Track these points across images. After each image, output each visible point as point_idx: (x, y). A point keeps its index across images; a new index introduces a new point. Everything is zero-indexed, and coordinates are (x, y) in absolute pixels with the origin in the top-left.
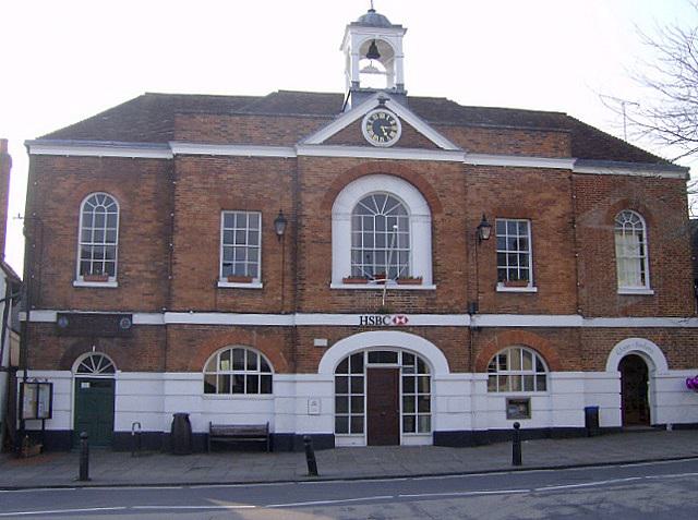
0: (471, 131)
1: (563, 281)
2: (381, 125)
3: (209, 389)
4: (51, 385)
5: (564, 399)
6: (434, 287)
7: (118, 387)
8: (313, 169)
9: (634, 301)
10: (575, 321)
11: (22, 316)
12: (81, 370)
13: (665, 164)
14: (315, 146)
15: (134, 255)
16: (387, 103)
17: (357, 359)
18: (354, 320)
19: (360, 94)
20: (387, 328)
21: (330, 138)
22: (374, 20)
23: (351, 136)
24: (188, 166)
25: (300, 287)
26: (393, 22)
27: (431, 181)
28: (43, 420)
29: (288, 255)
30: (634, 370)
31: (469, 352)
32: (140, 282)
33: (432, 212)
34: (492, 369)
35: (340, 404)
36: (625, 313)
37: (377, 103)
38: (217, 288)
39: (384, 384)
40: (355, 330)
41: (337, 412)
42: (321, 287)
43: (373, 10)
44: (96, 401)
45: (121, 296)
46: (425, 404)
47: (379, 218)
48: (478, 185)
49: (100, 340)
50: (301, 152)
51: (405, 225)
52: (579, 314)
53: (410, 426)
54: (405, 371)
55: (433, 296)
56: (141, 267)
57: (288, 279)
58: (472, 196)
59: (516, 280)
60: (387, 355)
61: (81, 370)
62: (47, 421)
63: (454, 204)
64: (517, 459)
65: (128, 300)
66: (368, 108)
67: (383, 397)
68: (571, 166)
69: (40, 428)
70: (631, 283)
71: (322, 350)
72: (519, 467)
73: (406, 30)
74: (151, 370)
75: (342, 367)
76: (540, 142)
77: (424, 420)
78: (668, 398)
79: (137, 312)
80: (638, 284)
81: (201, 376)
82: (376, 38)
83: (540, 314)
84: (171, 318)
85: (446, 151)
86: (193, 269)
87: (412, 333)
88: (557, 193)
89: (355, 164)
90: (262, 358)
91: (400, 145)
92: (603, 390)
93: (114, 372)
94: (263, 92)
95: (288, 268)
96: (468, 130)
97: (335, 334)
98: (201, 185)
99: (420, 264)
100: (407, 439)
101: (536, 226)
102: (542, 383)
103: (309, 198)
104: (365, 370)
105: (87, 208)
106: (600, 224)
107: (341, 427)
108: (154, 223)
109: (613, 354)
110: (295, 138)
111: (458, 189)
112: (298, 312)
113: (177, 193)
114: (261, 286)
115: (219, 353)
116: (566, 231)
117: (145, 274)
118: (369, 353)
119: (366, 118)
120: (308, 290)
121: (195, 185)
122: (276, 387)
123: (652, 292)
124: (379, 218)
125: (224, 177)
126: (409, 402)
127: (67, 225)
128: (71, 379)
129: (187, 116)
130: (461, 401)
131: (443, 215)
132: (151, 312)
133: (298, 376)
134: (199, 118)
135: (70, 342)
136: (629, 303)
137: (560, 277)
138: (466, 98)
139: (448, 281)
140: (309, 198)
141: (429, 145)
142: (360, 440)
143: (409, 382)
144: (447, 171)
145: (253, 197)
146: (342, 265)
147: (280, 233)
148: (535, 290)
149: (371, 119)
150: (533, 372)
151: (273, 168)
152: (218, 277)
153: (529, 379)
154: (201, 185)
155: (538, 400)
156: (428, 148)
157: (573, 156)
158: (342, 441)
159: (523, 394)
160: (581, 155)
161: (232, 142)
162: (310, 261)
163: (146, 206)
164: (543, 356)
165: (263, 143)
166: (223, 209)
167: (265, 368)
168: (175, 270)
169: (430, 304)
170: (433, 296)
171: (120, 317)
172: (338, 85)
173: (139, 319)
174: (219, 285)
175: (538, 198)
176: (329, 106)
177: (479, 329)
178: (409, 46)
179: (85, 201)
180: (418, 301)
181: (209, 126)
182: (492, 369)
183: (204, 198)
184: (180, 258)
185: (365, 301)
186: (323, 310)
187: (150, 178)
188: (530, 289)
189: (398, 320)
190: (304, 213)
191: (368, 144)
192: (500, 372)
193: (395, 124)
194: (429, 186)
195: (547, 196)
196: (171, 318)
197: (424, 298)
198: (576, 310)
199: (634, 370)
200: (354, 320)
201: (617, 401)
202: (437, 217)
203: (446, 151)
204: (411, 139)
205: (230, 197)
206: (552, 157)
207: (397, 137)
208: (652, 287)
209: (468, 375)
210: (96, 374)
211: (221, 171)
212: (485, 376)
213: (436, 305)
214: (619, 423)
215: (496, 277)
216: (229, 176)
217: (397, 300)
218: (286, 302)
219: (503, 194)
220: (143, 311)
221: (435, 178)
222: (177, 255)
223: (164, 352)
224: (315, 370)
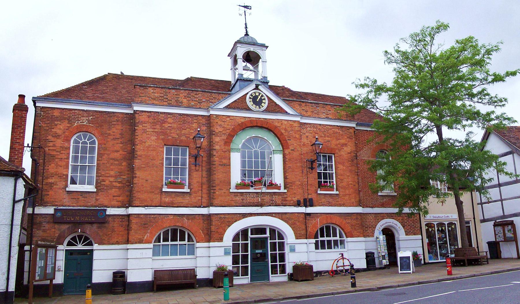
0: (304, 104)
1: (352, 188)
6: (286, 191)
8: (219, 123)
10: (358, 210)
11: (30, 211)
14: (220, 109)
15: (107, 172)
16: (260, 87)
17: (244, 233)
19: (243, 81)
21: (229, 105)
22: (246, 40)
23: (240, 105)
25: (212, 191)
26: (260, 41)
27: (283, 131)
30: (389, 233)
31: (303, 227)
32: (111, 188)
33: (283, 148)
34: (316, 237)
36: (383, 205)
37: (254, 86)
38: (162, 192)
40: (251, 215)
44: (80, 264)
45: (98, 198)
48: (307, 134)
50: (212, 112)
52: (360, 206)
53: (274, 272)
55: (285, 196)
56: (112, 179)
58: (304, 140)
60: (261, 230)
61: (69, 244)
63: (295, 144)
64: (354, 285)
65: (103, 199)
67: (259, 253)
68: (354, 125)
73: (267, 47)
74: (118, 243)
75: (236, 238)
81: (314, 241)
83: (341, 206)
84: (132, 210)
85: (291, 115)
86: (147, 180)
88: (348, 140)
89: (243, 121)
91: (267, 111)
93: (92, 245)
95: (205, 180)
96: (302, 104)
98: (152, 130)
99: (278, 178)
100: (274, 278)
101: (337, 158)
103: (217, 139)
104: (249, 239)
105: (76, 142)
106: (369, 157)
108: (121, 152)
109: (377, 227)
111: (297, 136)
112: (212, 206)
113: (136, 134)
114: (189, 191)
116: (353, 161)
117: (114, 184)
119: (250, 93)
120: (217, 193)
121: (148, 130)
123: (95, 190)
125: (166, 125)
127: (62, 152)
129: (142, 88)
131: (289, 150)
132: (118, 207)
133: (212, 244)
134: (151, 90)
136: (385, 200)
137: (350, 186)
138: (295, 88)
139: (293, 187)
143: (273, 245)
145: (183, 138)
146: (236, 177)
148: (338, 192)
149: (251, 95)
150: (338, 238)
151: (196, 121)
152: (163, 186)
154: (152, 130)
156: (281, 113)
161: (170, 105)
162: (218, 176)
163: (116, 142)
164: (343, 229)
165: (189, 107)
166: (165, 145)
168: (136, 181)
170: (285, 196)
172: (227, 76)
173: (110, 211)
174: (164, 190)
175: (338, 142)
176: (223, 88)
177: (309, 214)
178: (266, 55)
179: (74, 137)
180: (276, 198)
184: (138, 173)
185: (249, 199)
186: (226, 204)
187: (118, 125)
188: (335, 192)
190: (214, 148)
191: (248, 109)
192: (320, 239)
194: (282, 134)
195: (342, 141)
196: (132, 210)
197: (280, 197)
198: (360, 204)
199: (389, 233)
202: (287, 152)
204: (273, 108)
205: (169, 138)
206: (345, 120)
209: (305, 241)
210: (80, 247)
211: (164, 122)
212: (314, 241)
214: (365, 266)
215: (317, 186)
216: (169, 125)
217: (267, 198)
221: (286, 130)
222: (136, 172)
223: (126, 232)
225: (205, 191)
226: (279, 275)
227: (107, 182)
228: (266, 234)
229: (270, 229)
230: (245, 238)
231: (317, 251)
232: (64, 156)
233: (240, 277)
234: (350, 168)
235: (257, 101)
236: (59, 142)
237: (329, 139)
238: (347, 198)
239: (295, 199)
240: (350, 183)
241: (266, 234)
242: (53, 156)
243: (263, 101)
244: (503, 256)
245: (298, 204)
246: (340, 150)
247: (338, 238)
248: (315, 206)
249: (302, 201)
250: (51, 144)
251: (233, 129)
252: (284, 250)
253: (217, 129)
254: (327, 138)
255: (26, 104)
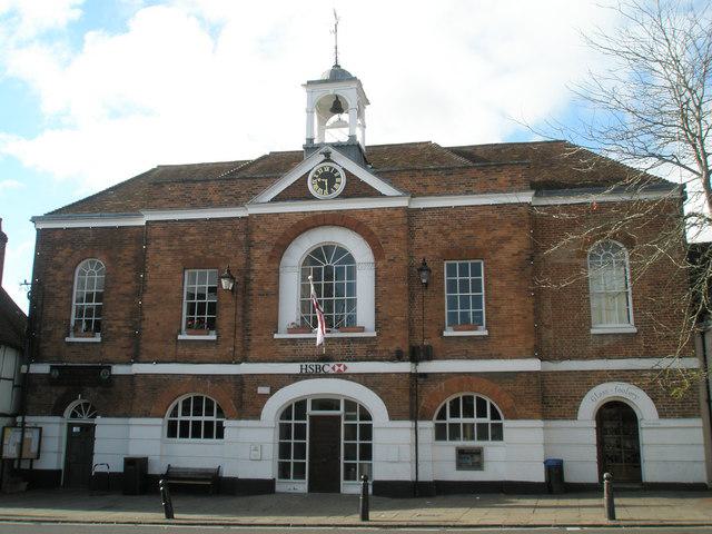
2: (328, 178)
3: (172, 433)
4: (41, 428)
5: (518, 450)
7: (99, 432)
9: (612, 340)
10: (533, 365)
11: (24, 369)
12: (74, 415)
13: (664, 185)
14: (264, 205)
18: (294, 368)
20: (327, 375)
22: (338, 75)
23: (298, 192)
24: (157, 231)
27: (374, 229)
28: (32, 460)
29: (240, 309)
30: (617, 424)
31: (410, 400)
35: (284, 451)
36: (601, 355)
37: (323, 157)
38: (178, 341)
39: (325, 429)
40: (296, 378)
41: (280, 458)
42: (265, 336)
43: (337, 66)
44: (81, 443)
46: (367, 452)
47: (328, 273)
49: (88, 388)
51: (352, 275)
52: (536, 357)
53: (350, 476)
54: (347, 418)
55: (373, 343)
56: (120, 323)
57: (239, 331)
58: (420, 240)
59: (468, 323)
62: (35, 462)
65: (110, 353)
66: (314, 164)
69: (28, 467)
70: (612, 316)
71: (265, 397)
72: (365, 523)
75: (286, 414)
76: (494, 177)
77: (366, 468)
78: (668, 445)
79: (114, 363)
80: (621, 321)
82: (336, 93)
85: (390, 197)
87: (352, 380)
90: (492, 406)
91: (344, 195)
92: (578, 443)
94: (253, 156)
97: (590, 379)
99: (365, 314)
102: (498, 434)
103: (257, 253)
107: (284, 471)
110: (251, 195)
115: (180, 401)
117: (123, 330)
118: (313, 401)
122: (226, 431)
123: (635, 330)
124: (328, 273)
125: (187, 239)
126: (350, 451)
128: (61, 423)
130: (396, 448)
135: (61, 391)
136: (606, 343)
140: (257, 253)
141: (372, 193)
142: (302, 486)
143: (351, 430)
144: (390, 217)
145: (210, 256)
146: (290, 310)
147: (424, 281)
153: (483, 427)
155: (491, 449)
157: (532, 189)
158: (283, 486)
159: (476, 443)
160: (540, 188)
161: (194, 206)
162: (257, 313)
167: (495, 415)
169: (370, 351)
171: (101, 368)
173: (118, 370)
177: (424, 375)
180: (359, 349)
181: (175, 194)
182: (442, 416)
183: (170, 259)
188: (482, 332)
189: (337, 368)
192: (449, 420)
193: (339, 176)
194: (372, 233)
195: (500, 233)
197: (365, 346)
199: (617, 424)
200: (294, 368)
201: (592, 454)
202: (380, 264)
203: (390, 197)
204: (356, 189)
205: (191, 257)
207: (340, 188)
208: (636, 325)
210: (85, 420)
211: (185, 233)
213: (376, 351)
218: (237, 352)
219: (453, 236)
220: (121, 363)
221: (379, 226)
223: (124, 399)
224: (257, 416)
225: (239, 338)
226: (292, 480)
227: (114, 329)
228: (451, 417)
229: (345, 400)
230: (301, 414)
231: (209, 440)
232: (64, 294)
233: (292, 480)
234: (517, 284)
235: (328, 178)
236: (60, 276)
237: (472, 231)
238: (506, 342)
239: (393, 349)
240: (516, 312)
241: (451, 417)
242: (52, 295)
243: (337, 180)
244: (650, 473)
245: (398, 357)
246: (494, 251)
247: (487, 420)
248: (437, 359)
249: (406, 349)
250: (51, 278)
251: (285, 234)
252: (370, 438)
253: (258, 237)
254: (467, 231)
255: (3, 230)
